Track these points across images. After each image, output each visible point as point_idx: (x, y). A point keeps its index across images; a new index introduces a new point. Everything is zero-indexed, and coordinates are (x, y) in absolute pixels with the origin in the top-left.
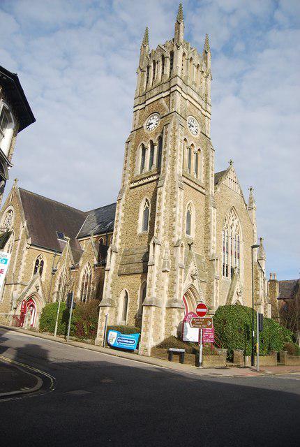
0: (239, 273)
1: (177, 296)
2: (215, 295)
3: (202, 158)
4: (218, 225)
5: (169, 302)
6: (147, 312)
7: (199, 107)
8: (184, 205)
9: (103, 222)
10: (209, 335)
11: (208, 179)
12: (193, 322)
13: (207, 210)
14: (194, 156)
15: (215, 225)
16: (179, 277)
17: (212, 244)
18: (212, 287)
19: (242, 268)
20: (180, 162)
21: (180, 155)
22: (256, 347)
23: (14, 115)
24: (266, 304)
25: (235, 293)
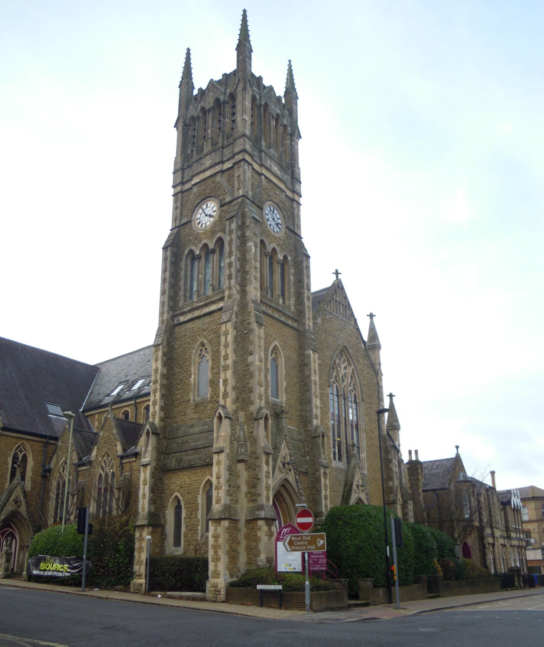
0: (359, 453)
1: (263, 500)
2: (323, 494)
4: (321, 378)
5: (252, 511)
6: (216, 530)
7: (282, 186)
8: (266, 350)
9: (127, 381)
10: (318, 559)
12: (291, 543)
14: (278, 269)
15: (317, 379)
16: (265, 468)
17: (314, 410)
18: (318, 480)
19: (364, 444)
20: (255, 278)
21: (255, 268)
22: (393, 571)
25: (354, 487)
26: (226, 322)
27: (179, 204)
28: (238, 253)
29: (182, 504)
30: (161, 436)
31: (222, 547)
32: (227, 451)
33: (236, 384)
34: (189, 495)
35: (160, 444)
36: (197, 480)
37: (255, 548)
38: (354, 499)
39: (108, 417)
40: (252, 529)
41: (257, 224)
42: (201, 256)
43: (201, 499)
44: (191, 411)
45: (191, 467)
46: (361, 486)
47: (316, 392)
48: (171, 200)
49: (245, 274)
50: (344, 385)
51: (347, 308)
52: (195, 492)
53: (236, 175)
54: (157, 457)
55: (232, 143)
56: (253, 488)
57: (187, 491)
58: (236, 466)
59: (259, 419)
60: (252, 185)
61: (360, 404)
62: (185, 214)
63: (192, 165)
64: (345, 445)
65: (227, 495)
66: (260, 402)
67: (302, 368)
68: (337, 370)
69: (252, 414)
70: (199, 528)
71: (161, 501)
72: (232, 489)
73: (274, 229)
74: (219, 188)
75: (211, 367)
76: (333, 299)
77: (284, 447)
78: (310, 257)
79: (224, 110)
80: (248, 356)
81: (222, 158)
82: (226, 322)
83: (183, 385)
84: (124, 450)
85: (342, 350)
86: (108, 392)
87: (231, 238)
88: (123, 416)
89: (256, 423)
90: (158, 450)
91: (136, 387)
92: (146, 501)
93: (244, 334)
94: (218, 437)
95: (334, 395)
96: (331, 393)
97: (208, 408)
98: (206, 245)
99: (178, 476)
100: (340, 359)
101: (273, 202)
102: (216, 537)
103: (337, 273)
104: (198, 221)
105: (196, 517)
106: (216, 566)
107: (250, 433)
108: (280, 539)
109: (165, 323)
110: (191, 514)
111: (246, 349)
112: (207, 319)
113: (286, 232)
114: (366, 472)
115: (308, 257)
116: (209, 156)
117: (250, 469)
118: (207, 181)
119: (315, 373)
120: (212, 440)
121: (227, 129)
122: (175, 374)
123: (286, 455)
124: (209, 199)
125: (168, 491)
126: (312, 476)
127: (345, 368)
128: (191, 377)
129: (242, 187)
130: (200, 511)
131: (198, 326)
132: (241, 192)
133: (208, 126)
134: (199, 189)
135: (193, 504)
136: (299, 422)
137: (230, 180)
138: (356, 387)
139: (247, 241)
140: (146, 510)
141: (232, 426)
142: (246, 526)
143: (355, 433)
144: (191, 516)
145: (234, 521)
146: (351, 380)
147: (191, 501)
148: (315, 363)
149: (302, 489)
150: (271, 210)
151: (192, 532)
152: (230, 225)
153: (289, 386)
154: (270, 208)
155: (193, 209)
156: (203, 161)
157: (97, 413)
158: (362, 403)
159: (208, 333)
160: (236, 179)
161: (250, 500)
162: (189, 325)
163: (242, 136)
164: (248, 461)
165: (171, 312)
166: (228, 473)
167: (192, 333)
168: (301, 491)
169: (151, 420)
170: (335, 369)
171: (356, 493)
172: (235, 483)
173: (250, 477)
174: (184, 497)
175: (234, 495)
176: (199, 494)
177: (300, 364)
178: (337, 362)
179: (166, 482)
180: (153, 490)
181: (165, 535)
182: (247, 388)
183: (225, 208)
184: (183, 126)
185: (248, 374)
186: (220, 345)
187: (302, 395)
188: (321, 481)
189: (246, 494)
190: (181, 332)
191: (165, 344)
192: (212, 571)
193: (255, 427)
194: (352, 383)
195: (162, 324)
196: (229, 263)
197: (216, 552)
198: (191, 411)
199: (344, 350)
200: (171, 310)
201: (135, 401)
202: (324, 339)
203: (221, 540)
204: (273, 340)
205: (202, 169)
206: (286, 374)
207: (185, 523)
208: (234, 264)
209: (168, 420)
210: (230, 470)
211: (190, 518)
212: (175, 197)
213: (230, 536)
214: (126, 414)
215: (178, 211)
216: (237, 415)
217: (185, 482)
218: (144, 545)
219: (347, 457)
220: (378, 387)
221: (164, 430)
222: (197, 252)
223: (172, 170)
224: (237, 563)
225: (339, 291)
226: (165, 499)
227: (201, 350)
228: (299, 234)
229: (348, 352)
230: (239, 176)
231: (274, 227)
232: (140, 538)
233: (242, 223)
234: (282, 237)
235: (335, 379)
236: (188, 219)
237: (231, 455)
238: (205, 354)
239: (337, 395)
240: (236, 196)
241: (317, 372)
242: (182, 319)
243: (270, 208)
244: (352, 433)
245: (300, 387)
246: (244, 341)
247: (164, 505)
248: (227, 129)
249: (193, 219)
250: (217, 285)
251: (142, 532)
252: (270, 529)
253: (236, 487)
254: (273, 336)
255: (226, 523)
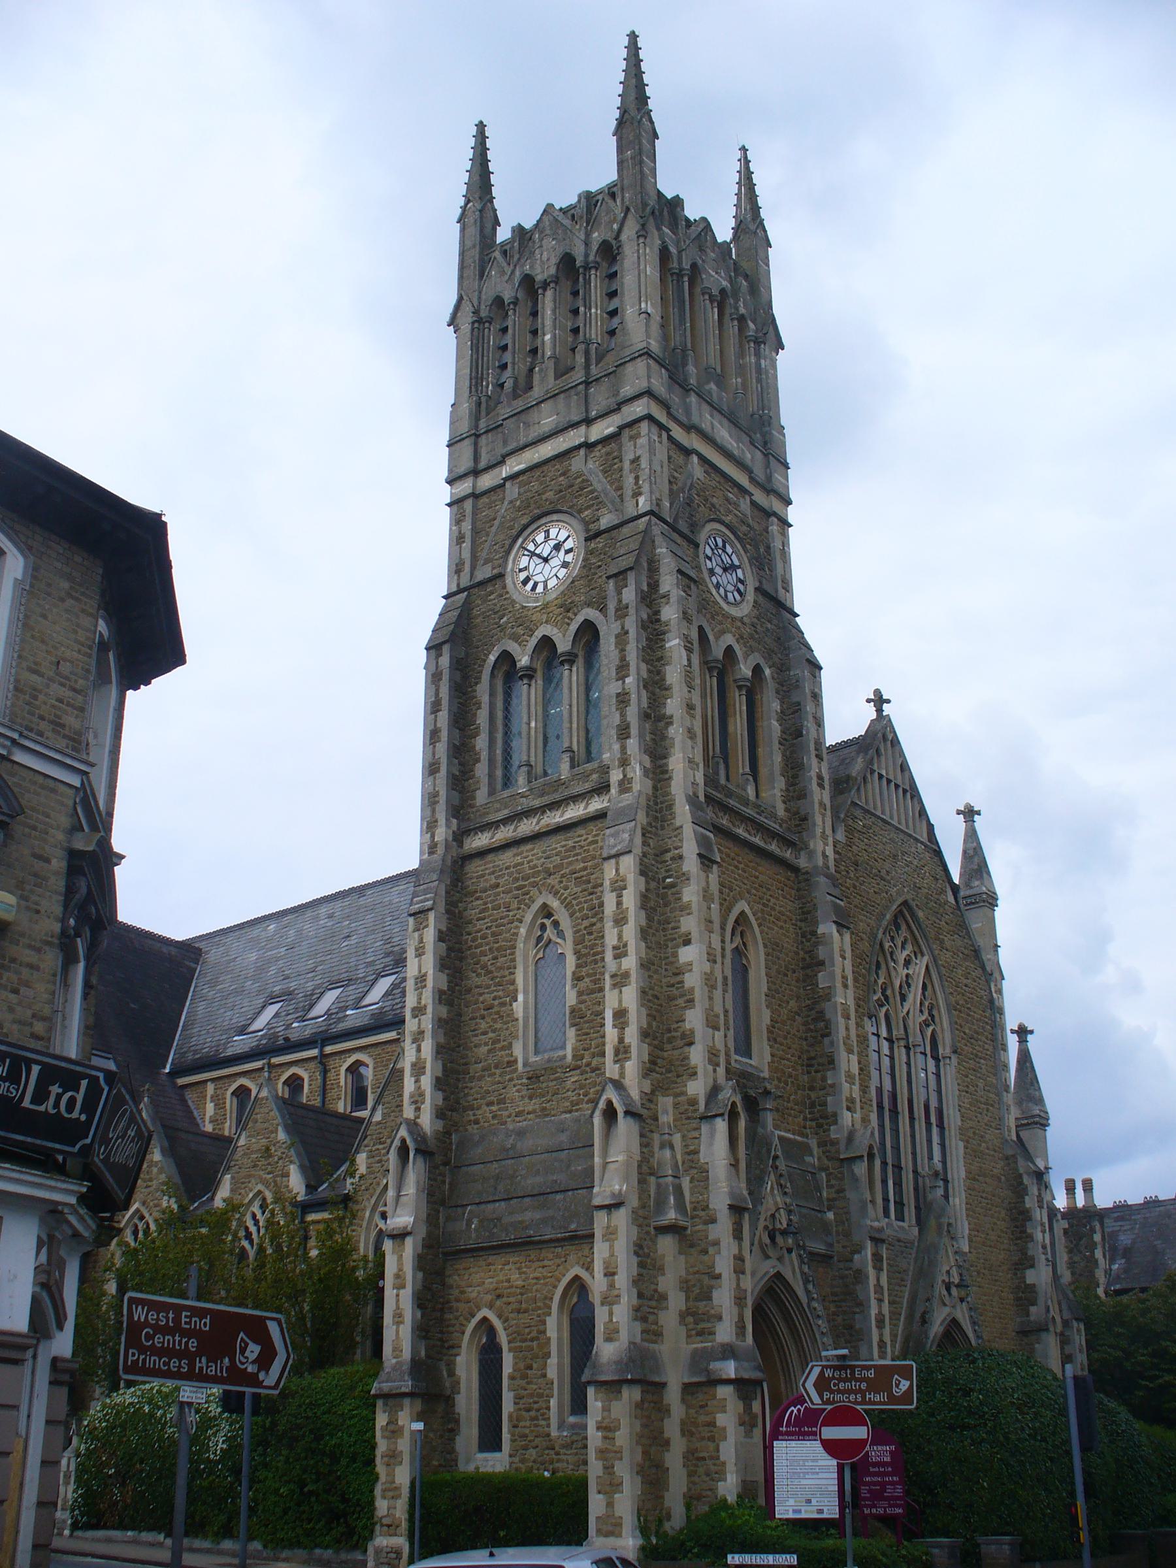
0: (946, 1197)
2: (874, 1312)
3: (771, 704)
5: (699, 1360)
6: (607, 1409)
10: (883, 1485)
11: (802, 795)
13: (809, 937)
14: (739, 703)
15: (851, 1002)
19: (958, 1172)
23: (118, 658)
24: (1066, 1323)
26: (617, 856)
27: (467, 526)
28: (644, 666)
29: (503, 1338)
30: (438, 1159)
31: (626, 1454)
32: (634, 1201)
33: (650, 1025)
34: (521, 1316)
35: (435, 1180)
36: (545, 1278)
37: (712, 1458)
38: (938, 1322)
39: (260, 1096)
40: (702, 1407)
41: (689, 587)
42: (535, 671)
43: (555, 1328)
44: (518, 1091)
45: (524, 1245)
46: (957, 1286)
47: (848, 1037)
48: (444, 516)
49: (662, 724)
50: (905, 1011)
51: (908, 795)
52: (539, 1308)
53: (628, 456)
54: (429, 1215)
55: (614, 371)
56: (701, 1300)
57: (514, 1306)
58: (654, 1242)
59: (716, 1116)
60: (670, 482)
61: (948, 1061)
62: (484, 555)
63: (502, 425)
64: (911, 1176)
65: (635, 1319)
66: (715, 1071)
67: (808, 971)
68: (888, 969)
69: (693, 1102)
70: (553, 1403)
71: (441, 1332)
72: (645, 1302)
73: (726, 596)
74: (582, 489)
75: (574, 973)
76: (872, 772)
77: (772, 1187)
78: (820, 668)
79: (587, 282)
80: (678, 946)
81: (587, 411)
82: (617, 856)
83: (494, 1021)
84: (311, 1188)
85: (899, 914)
86: (241, 1021)
87: (623, 628)
88: (287, 1089)
89: (705, 1128)
90: (430, 1194)
91: (321, 1008)
92: (406, 1331)
93: (663, 888)
94: (605, 1165)
95: (881, 1039)
96: (873, 1034)
97: (569, 1084)
98: (546, 642)
99: (490, 1264)
100: (892, 939)
101: (722, 523)
102: (608, 1428)
103: (879, 700)
104: (523, 576)
105: (544, 1376)
106: (610, 1505)
107: (689, 1154)
108: (782, 1434)
109: (440, 850)
110: (530, 1368)
111: (673, 928)
112: (557, 843)
113: (755, 602)
114: (966, 1249)
115: (816, 667)
116: (550, 403)
117: (692, 1250)
118: (545, 468)
119: (845, 986)
120: (590, 1171)
121: (595, 332)
122: (469, 991)
123: (778, 1209)
124: (555, 517)
125: (461, 1306)
126: (841, 1265)
127: (907, 963)
128: (516, 1000)
129: (646, 488)
130: (553, 1361)
131: (531, 861)
132: (643, 503)
133: (543, 324)
134: (522, 490)
135: (532, 1340)
136: (805, 1119)
137: (611, 467)
138: (935, 1012)
139: (664, 634)
140: (407, 1354)
141: (642, 1135)
142: (683, 1400)
143: (936, 1139)
144: (529, 1372)
145: (653, 1388)
146: (923, 994)
147: (529, 1333)
148: (844, 958)
149: (817, 1300)
150: (717, 545)
151: (533, 1413)
152: (619, 593)
153: (777, 1022)
154: (715, 538)
155: (507, 542)
156: (534, 415)
157: (213, 1080)
158: (954, 1057)
159: (561, 882)
160: (627, 465)
161: (694, 1332)
162: (507, 857)
163: (640, 356)
164: (685, 1228)
165: (455, 821)
166: (635, 1260)
167: (517, 880)
168: (815, 1304)
169: (408, 1112)
170: (883, 966)
171: (945, 1305)
172: (653, 1287)
173: (691, 1270)
174: (506, 1320)
175: (651, 1318)
176: (549, 1314)
177: (804, 959)
178: (887, 945)
179: (454, 1280)
180: (422, 1300)
181: (457, 1421)
182: (679, 1034)
183: (599, 543)
184: (473, 323)
185: (681, 996)
186: (601, 920)
187: (812, 1045)
188: (868, 1278)
189: (683, 1316)
190: (483, 876)
191: (441, 907)
192: (597, 1518)
193: (703, 1138)
194: (927, 1004)
195: (430, 853)
196: (618, 695)
197: (608, 1469)
198: (518, 1091)
199: (904, 914)
200: (454, 817)
201: (321, 1051)
202: (855, 887)
203: (623, 1438)
204: (736, 901)
205: (530, 439)
206: (769, 989)
207: (510, 1390)
208: (634, 697)
209: (454, 1114)
210: (641, 1252)
211: (524, 1377)
212: (455, 507)
213: (644, 1426)
214: (295, 1083)
215: (467, 545)
216: (652, 1106)
217: (508, 1281)
218: (404, 1445)
219: (917, 1208)
220: (993, 1009)
221: (445, 1142)
222: (524, 661)
223: (446, 438)
224: (662, 1497)
225: (886, 750)
226: (454, 1325)
227: (543, 927)
228: (788, 604)
229: (913, 915)
230: (636, 460)
231: (726, 591)
232: (391, 1427)
233: (649, 585)
234: (746, 616)
235: (883, 993)
236: (493, 568)
237: (641, 1212)
238: (554, 938)
239: (890, 1040)
240: (631, 511)
241: (850, 982)
242: (481, 841)
243: (715, 538)
244: (930, 1141)
245: (805, 1024)
246: (666, 905)
247: (451, 1342)
248: (595, 332)
249: (509, 569)
250: (583, 750)
251: (396, 1412)
252: (748, 1408)
253: (656, 1297)
254: (735, 887)
255: (630, 1395)
